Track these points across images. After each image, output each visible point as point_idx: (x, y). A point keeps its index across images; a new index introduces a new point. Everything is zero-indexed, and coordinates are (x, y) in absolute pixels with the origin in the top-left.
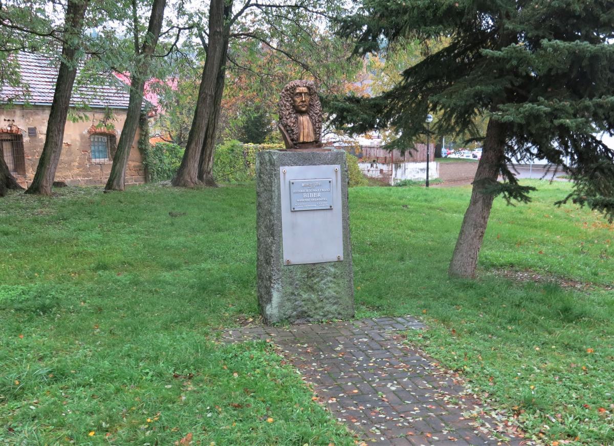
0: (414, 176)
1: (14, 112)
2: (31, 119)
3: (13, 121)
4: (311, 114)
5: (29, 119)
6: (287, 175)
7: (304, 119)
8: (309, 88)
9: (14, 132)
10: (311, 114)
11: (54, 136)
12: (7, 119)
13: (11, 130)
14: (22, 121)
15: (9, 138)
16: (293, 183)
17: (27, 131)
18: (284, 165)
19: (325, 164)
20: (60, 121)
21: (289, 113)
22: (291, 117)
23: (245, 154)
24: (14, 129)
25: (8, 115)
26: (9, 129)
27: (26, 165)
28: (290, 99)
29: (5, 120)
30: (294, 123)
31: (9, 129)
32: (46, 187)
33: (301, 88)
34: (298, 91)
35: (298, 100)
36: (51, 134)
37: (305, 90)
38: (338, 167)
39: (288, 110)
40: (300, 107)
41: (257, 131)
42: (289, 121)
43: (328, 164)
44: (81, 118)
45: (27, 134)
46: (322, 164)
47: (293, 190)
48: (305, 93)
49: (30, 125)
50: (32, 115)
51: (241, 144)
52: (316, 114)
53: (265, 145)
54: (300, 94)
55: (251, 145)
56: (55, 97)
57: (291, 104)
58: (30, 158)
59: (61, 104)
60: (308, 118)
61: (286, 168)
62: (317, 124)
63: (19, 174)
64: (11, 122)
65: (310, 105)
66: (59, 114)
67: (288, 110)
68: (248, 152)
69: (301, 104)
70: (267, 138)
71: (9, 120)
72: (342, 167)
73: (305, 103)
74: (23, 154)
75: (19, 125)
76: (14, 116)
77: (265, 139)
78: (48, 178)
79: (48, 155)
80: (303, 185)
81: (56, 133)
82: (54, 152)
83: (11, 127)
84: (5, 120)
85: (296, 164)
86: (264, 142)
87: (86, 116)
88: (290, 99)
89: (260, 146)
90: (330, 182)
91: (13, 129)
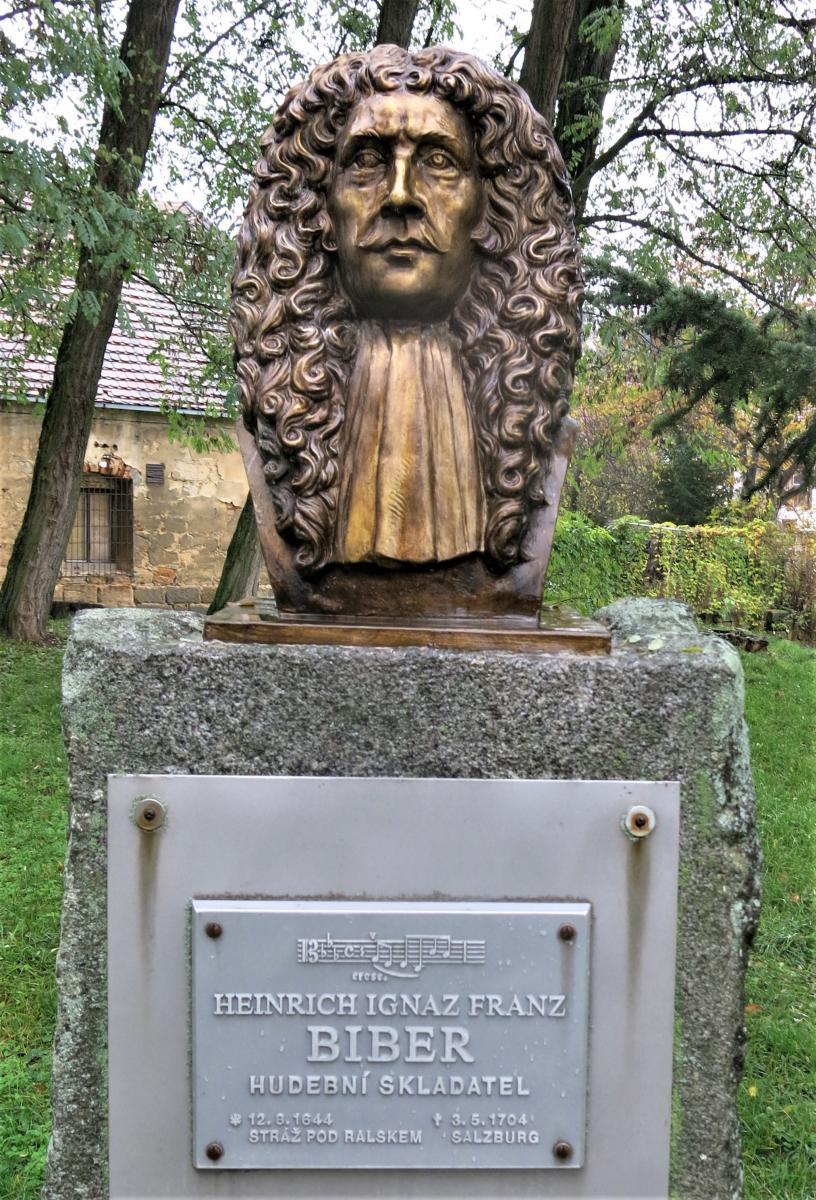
0: (612, 122)
1: (119, 428)
2: (155, 444)
3: (115, 447)
4: (473, 333)
5: (150, 445)
6: (169, 847)
7: (399, 368)
8: (466, 105)
9: (115, 472)
10: (473, 333)
11: (51, 480)
12: (101, 443)
13: (108, 468)
14: (134, 448)
15: (104, 486)
16: (214, 932)
17: (144, 472)
18: (154, 757)
19: (533, 766)
20: (68, 438)
21: (289, 318)
22: (295, 348)
23: (652, 549)
24: (115, 465)
25: (103, 433)
26: (104, 464)
27: (136, 548)
28: (308, 199)
29: (97, 445)
30: (316, 398)
31: (104, 464)
32: (25, 618)
33: (391, 103)
34: (360, 125)
35: (360, 201)
36: (42, 475)
37: (428, 116)
38: (656, 798)
39: (279, 286)
40: (377, 262)
41: (691, 495)
42: (277, 372)
43: (564, 771)
44: (215, 441)
45: (143, 477)
46: (505, 765)
47: (213, 995)
48: (426, 144)
49: (152, 458)
50: (157, 437)
51: (645, 522)
52: (525, 328)
53: (705, 529)
54: (383, 145)
55: (669, 527)
56: (56, 374)
57: (314, 243)
58: (145, 532)
59: (69, 392)
60: (440, 357)
61: (172, 787)
62: (514, 414)
63: (119, 568)
64: (108, 451)
65: (478, 251)
66: (65, 420)
67: (279, 286)
68: (660, 544)
69: (381, 233)
70: (715, 513)
71: (105, 446)
72: (690, 806)
73: (418, 231)
74: (131, 523)
75: (126, 458)
76: (118, 436)
77: (708, 514)
78: (32, 595)
79: (35, 531)
80: (310, 946)
81: (57, 473)
82: (50, 524)
83: (108, 460)
84: (97, 445)
85: (262, 757)
86: (703, 522)
87: (226, 438)
88: (308, 199)
89: (692, 530)
90: (567, 935)
91: (112, 466)
